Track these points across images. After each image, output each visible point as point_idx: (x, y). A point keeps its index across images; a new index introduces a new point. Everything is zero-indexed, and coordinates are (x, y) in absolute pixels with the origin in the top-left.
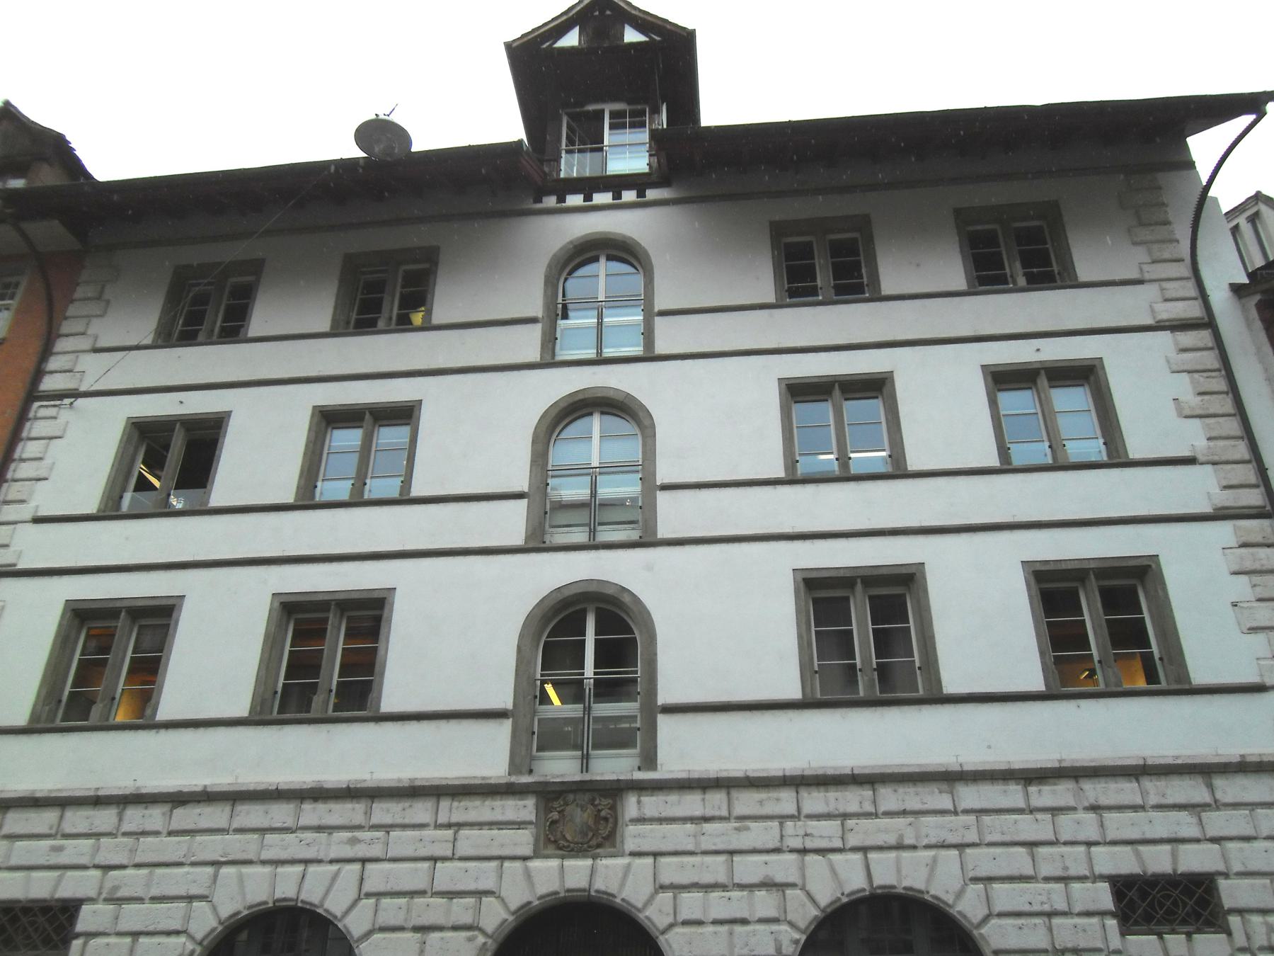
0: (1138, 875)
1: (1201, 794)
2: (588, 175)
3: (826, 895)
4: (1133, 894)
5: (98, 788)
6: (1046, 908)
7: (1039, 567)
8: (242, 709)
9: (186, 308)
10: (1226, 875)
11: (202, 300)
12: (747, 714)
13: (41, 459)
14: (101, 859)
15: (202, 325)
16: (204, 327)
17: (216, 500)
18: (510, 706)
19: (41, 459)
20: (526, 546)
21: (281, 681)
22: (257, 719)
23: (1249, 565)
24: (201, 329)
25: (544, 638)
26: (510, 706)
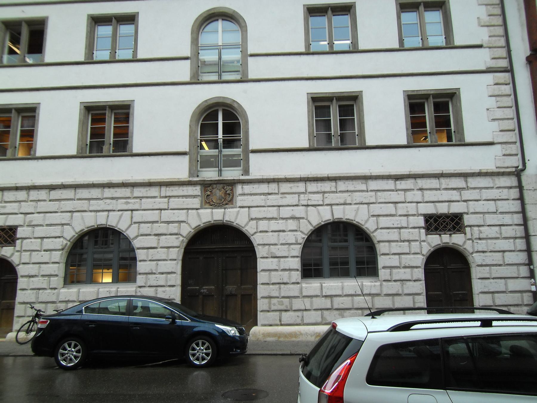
0: (435, 214)
10: (467, 214)
12: (286, 153)
23: (496, 93)
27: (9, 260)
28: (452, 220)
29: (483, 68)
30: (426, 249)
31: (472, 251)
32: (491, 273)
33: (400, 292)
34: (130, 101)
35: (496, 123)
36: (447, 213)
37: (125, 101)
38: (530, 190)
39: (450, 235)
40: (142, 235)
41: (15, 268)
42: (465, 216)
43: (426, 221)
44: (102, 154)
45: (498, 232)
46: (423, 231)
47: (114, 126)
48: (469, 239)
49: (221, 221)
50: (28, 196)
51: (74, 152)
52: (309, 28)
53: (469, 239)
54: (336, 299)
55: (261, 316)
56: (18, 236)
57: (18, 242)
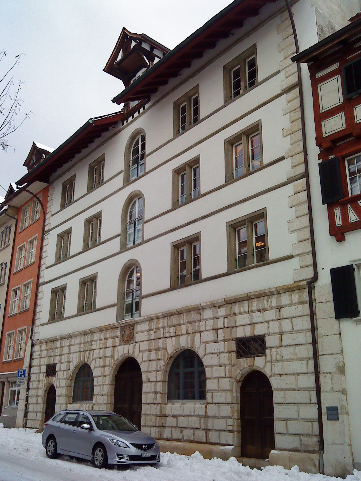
0: (244, 337)
1: (197, 317)
2: (135, 102)
3: (171, 350)
4: (260, 342)
5: (277, 287)
6: (218, 351)
7: (232, 223)
8: (167, 285)
9: (232, 82)
10: (269, 335)
11: (237, 74)
12: (286, 261)
13: (46, 251)
14: (266, 319)
15: (240, 87)
16: (241, 88)
17: (267, 159)
18: (116, 303)
19: (46, 251)
20: (121, 251)
21: (237, 256)
22: (173, 288)
23: (295, 202)
24: (240, 89)
25: (127, 279)
26: (116, 303)
27: (263, 371)
28: (49, 368)
29: (285, 179)
30: (238, 373)
31: (271, 374)
32: (285, 398)
33: (217, 415)
34: (231, 222)
35: (295, 234)
36: (253, 335)
37: (190, 236)
38: (322, 303)
39: (254, 357)
40: (144, 361)
41: (269, 380)
42: (267, 338)
43: (238, 345)
44: (246, 267)
45: (292, 352)
46: (234, 355)
47: (255, 237)
48: (269, 362)
49: (127, 354)
50: (200, 316)
51: (225, 270)
52: (128, 212)
53: (269, 362)
54: (180, 419)
55: (279, 440)
56: (267, 345)
57: (268, 351)
